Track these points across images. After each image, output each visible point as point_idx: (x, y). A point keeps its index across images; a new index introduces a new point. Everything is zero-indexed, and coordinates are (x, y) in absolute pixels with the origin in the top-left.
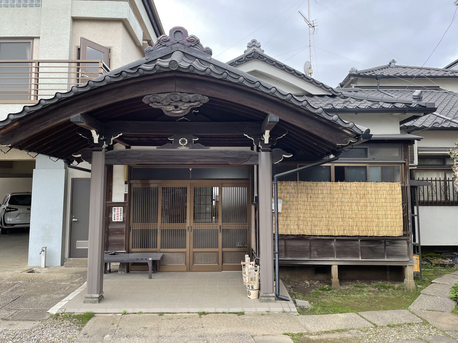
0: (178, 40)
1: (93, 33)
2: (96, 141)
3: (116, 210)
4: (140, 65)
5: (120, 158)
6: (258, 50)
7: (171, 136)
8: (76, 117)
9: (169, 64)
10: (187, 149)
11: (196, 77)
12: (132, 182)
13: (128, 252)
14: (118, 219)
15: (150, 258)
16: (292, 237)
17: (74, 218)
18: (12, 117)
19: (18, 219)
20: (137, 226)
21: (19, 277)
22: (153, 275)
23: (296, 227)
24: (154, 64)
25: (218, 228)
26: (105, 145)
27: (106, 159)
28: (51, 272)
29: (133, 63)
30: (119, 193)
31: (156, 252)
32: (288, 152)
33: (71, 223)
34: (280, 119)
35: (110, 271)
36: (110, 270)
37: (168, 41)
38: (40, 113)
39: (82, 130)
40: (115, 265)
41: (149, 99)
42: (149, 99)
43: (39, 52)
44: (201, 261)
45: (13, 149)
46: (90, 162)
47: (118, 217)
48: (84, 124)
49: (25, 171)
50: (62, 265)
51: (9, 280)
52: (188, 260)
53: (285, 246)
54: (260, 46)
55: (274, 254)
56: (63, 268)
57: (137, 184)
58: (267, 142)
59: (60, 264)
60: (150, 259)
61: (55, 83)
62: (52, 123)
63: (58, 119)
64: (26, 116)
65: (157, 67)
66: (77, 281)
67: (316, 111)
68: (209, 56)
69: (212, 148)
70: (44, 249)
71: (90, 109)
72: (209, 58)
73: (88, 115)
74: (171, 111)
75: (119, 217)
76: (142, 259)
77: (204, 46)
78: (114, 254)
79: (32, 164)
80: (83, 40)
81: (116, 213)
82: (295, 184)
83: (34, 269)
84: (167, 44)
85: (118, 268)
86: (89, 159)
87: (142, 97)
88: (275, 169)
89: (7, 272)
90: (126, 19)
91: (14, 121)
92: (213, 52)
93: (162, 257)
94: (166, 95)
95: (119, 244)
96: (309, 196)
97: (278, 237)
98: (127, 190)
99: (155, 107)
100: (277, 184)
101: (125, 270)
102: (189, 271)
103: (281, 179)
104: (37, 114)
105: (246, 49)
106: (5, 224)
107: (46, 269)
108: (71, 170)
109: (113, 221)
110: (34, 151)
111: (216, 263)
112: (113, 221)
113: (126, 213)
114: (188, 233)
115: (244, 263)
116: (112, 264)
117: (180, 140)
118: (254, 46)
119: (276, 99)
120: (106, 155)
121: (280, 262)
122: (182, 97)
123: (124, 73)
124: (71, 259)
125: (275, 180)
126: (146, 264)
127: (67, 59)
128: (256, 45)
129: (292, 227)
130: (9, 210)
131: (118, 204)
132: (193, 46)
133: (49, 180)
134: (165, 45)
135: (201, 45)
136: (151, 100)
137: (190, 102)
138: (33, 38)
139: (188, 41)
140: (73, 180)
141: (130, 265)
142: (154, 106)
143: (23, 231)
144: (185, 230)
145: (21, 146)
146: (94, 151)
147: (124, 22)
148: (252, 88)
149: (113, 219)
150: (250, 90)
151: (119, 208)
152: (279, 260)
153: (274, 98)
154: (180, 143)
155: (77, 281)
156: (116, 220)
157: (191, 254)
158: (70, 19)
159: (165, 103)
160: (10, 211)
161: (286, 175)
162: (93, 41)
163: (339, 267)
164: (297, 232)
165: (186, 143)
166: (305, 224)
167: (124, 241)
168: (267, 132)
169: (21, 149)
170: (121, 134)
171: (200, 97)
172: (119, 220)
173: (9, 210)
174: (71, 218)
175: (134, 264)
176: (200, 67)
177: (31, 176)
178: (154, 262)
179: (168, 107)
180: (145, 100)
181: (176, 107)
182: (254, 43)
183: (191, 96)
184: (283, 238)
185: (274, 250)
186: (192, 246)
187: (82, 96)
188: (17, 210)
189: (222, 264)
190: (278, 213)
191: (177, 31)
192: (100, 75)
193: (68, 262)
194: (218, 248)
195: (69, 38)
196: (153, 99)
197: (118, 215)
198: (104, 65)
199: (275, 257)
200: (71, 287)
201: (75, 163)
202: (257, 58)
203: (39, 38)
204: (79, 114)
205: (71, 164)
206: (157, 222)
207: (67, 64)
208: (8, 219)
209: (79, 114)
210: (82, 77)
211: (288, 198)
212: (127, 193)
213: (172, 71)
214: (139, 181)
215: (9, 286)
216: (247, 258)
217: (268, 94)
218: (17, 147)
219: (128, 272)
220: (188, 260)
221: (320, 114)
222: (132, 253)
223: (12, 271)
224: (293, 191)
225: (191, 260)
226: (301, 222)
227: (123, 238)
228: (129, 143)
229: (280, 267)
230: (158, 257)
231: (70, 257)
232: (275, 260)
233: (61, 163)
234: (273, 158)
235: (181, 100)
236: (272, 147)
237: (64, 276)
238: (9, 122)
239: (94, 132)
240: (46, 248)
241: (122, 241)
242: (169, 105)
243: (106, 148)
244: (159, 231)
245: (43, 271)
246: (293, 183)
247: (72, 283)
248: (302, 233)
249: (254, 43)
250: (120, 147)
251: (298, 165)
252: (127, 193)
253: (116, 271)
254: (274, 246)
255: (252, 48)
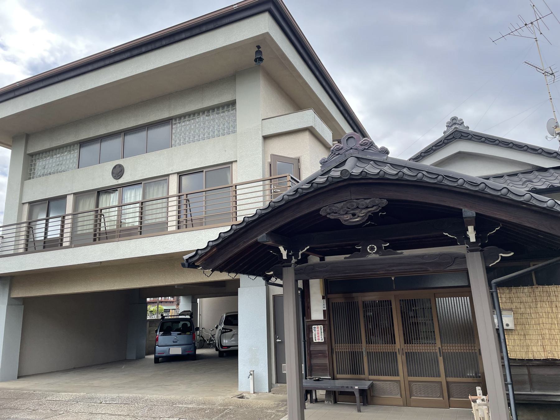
0: (351, 146)
1: (281, 148)
2: (285, 257)
3: (316, 329)
4: (315, 179)
5: (314, 272)
6: (460, 128)
7: (358, 244)
8: (262, 238)
9: (341, 173)
10: (377, 256)
11: (371, 181)
12: (329, 296)
13: (334, 378)
14: (319, 339)
15: (356, 386)
16: (537, 362)
17: (278, 338)
18: (211, 244)
19: (232, 341)
20: (342, 348)
21: (230, 403)
22: (362, 408)
23: (540, 349)
24: (327, 176)
25: (438, 351)
26: (294, 260)
27: (296, 274)
28: (259, 399)
29: (310, 177)
30: (317, 311)
31: (364, 379)
32: (507, 251)
33: (276, 343)
34: (476, 213)
35: (316, 401)
36: (316, 399)
37: (341, 149)
38: (233, 237)
39: (270, 247)
40: (321, 394)
41: (326, 210)
42: (326, 210)
43: (238, 175)
44: (420, 394)
45: (215, 272)
46: (282, 280)
47: (318, 337)
48: (270, 243)
49: (229, 290)
50: (270, 391)
51: (220, 405)
52: (403, 392)
53: (529, 374)
54: (463, 123)
55: (506, 385)
56: (271, 394)
57: (338, 299)
58: (473, 239)
59: (267, 391)
60: (356, 387)
61: (251, 202)
62: (243, 245)
63: (248, 241)
64: (222, 242)
65: (330, 179)
66: (282, 409)
67: (521, 199)
68: (385, 156)
69: (407, 253)
70: (252, 373)
71: (274, 228)
72: (385, 158)
73: (271, 234)
74: (348, 220)
75: (320, 336)
76: (347, 387)
77: (379, 146)
78: (318, 380)
79: (236, 283)
80: (273, 156)
81: (316, 333)
82: (530, 290)
83: (244, 394)
84: (341, 152)
85: (324, 397)
86: (279, 275)
87: (320, 209)
88: (491, 273)
89: (219, 397)
90: (312, 127)
91: (213, 247)
92: (390, 149)
93: (372, 386)
94: (342, 204)
95: (323, 369)
96: (554, 306)
97: (509, 363)
98: (325, 306)
99: (332, 218)
100: (497, 291)
101: (332, 399)
102: (407, 406)
103: (500, 285)
104: (230, 239)
105: (445, 129)
106: (222, 347)
107: (255, 395)
108: (271, 287)
109: (314, 341)
110: (233, 272)
111: (439, 397)
112: (314, 341)
113: (326, 332)
114: (399, 357)
115: (474, 397)
116: (177, 351)
117: (368, 247)
118: (455, 124)
119: (467, 191)
120: (295, 270)
121: (516, 397)
122: (358, 204)
123: (299, 190)
124: (279, 385)
125: (493, 287)
126: (352, 394)
127: (260, 177)
128: (458, 122)
129: (535, 349)
130: (224, 331)
131: (318, 322)
132: (367, 149)
133: (253, 297)
134: (339, 154)
135: (376, 147)
136: (328, 211)
137: (367, 208)
138: (231, 163)
139: (362, 145)
140: (274, 296)
141: (337, 394)
142: (332, 217)
143: (231, 354)
144: (396, 353)
145: (221, 269)
146: (284, 267)
147: (311, 130)
148: (435, 183)
149: (314, 339)
150: (433, 186)
151: (319, 326)
152: (514, 394)
153: (463, 191)
154: (369, 250)
155: (282, 409)
156: (317, 341)
157: (407, 383)
158: (261, 138)
159: (342, 212)
160: (226, 332)
161: (512, 277)
162: (283, 155)
163: (409, 376)
164: (542, 356)
165: (376, 250)
166: (554, 342)
167: (328, 364)
168: (471, 229)
169: (221, 272)
170: (308, 247)
171: (377, 201)
172: (320, 341)
173: (224, 331)
174: (275, 339)
175: (342, 393)
176: (372, 170)
177: (236, 294)
178: (362, 392)
179: (345, 216)
180: (322, 213)
181: (354, 215)
182: (454, 121)
183: (369, 201)
184: (515, 364)
185: (506, 380)
186: (406, 373)
187: (253, 224)
188: (231, 330)
189: (449, 399)
190: (503, 329)
191: (349, 138)
192: (289, 189)
193: (275, 388)
194: (439, 376)
195: (261, 156)
196: (330, 210)
197: (318, 335)
198: (292, 178)
199: (507, 390)
200: (277, 415)
201: (273, 280)
202: (460, 138)
203: (236, 161)
204: (264, 234)
205: (270, 281)
206: (395, 343)
207: (261, 183)
208: (224, 341)
209: (264, 234)
210: (275, 192)
211: (522, 310)
212: (325, 309)
213: (345, 180)
214: (341, 295)
215: (220, 411)
216: (479, 390)
217: (455, 187)
218: (217, 270)
219: (335, 402)
220: (403, 392)
221: (528, 201)
222: (337, 379)
223: (224, 396)
224: (529, 299)
225: (408, 393)
226: (546, 342)
227: (326, 361)
228: (323, 255)
229: (516, 404)
230: (366, 385)
231: (277, 382)
232: (508, 395)
233: (260, 280)
234: (486, 259)
235: (358, 207)
236: (483, 246)
237: (271, 403)
238: (209, 249)
239: (281, 248)
240: (253, 371)
241: (325, 365)
242: (346, 213)
243: (296, 263)
244: (364, 353)
245: (253, 397)
246: (526, 289)
247: (278, 411)
248: (550, 357)
249: (454, 121)
250: (314, 259)
251: (531, 264)
252: (325, 309)
253: (323, 401)
254: (505, 376)
255: (453, 127)
